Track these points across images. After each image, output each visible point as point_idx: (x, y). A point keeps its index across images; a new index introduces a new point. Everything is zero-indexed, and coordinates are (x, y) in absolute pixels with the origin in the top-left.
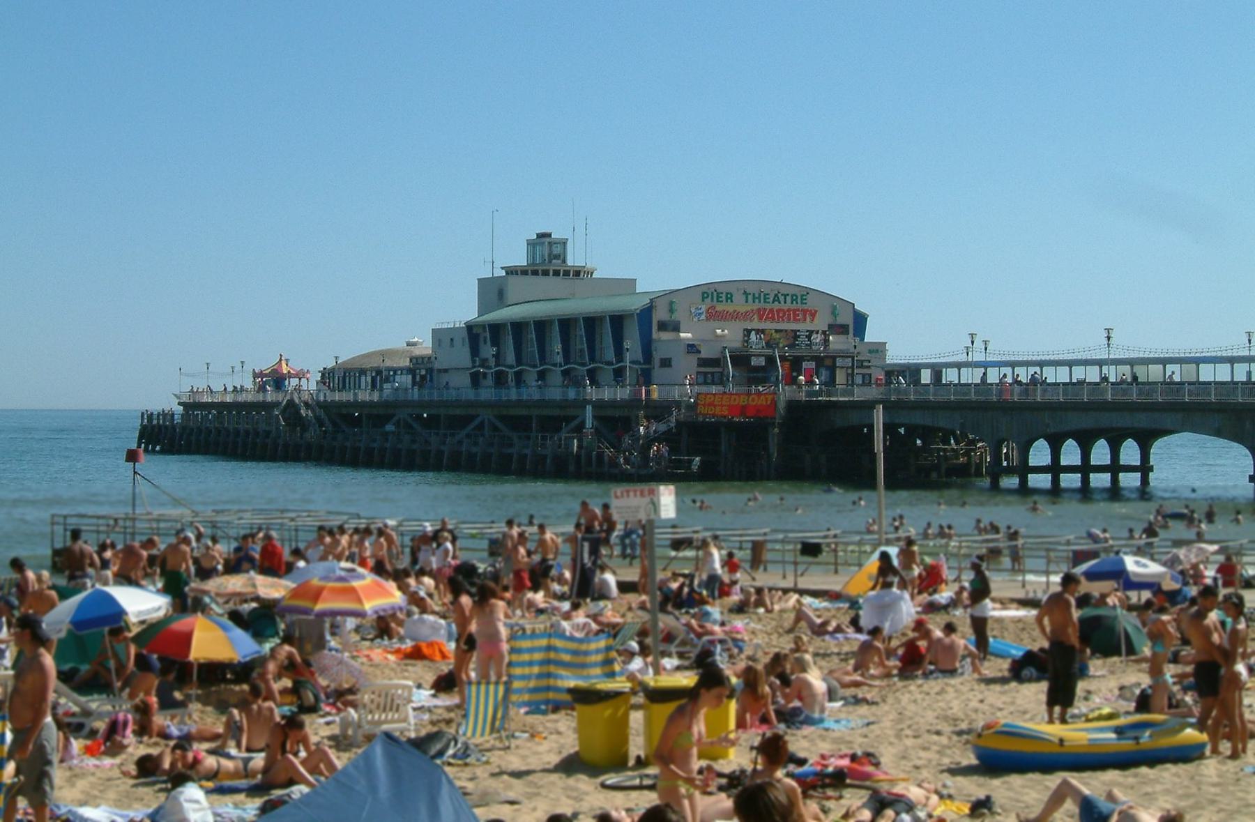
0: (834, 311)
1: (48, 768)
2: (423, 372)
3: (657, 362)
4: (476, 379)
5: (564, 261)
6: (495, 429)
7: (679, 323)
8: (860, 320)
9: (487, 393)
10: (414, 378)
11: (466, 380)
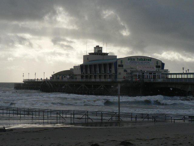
0: (157, 63)
1: (187, 56)
2: (72, 75)
3: (118, 74)
4: (82, 77)
5: (102, 52)
6: (85, 87)
7: (123, 65)
8: (163, 65)
9: (84, 80)
10: (70, 76)
11: (80, 77)
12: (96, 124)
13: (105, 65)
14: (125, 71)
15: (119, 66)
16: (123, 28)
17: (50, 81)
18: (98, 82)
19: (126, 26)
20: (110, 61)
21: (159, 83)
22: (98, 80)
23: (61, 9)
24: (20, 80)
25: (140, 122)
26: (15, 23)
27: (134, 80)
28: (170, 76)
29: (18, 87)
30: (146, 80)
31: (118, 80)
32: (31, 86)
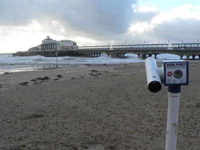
8: (76, 43)
9: (43, 51)
12: (48, 69)
13: (51, 44)
14: (60, 46)
15: (58, 44)
16: (61, 28)
17: (28, 52)
18: (49, 52)
19: (62, 28)
20: (54, 42)
21: (74, 51)
22: (49, 50)
23: (35, 21)
24: (15, 52)
25: (66, 67)
26: (15, 27)
27: (64, 50)
28: (79, 48)
29: (14, 55)
30: (69, 50)
31: (57, 50)
32: (20, 54)
